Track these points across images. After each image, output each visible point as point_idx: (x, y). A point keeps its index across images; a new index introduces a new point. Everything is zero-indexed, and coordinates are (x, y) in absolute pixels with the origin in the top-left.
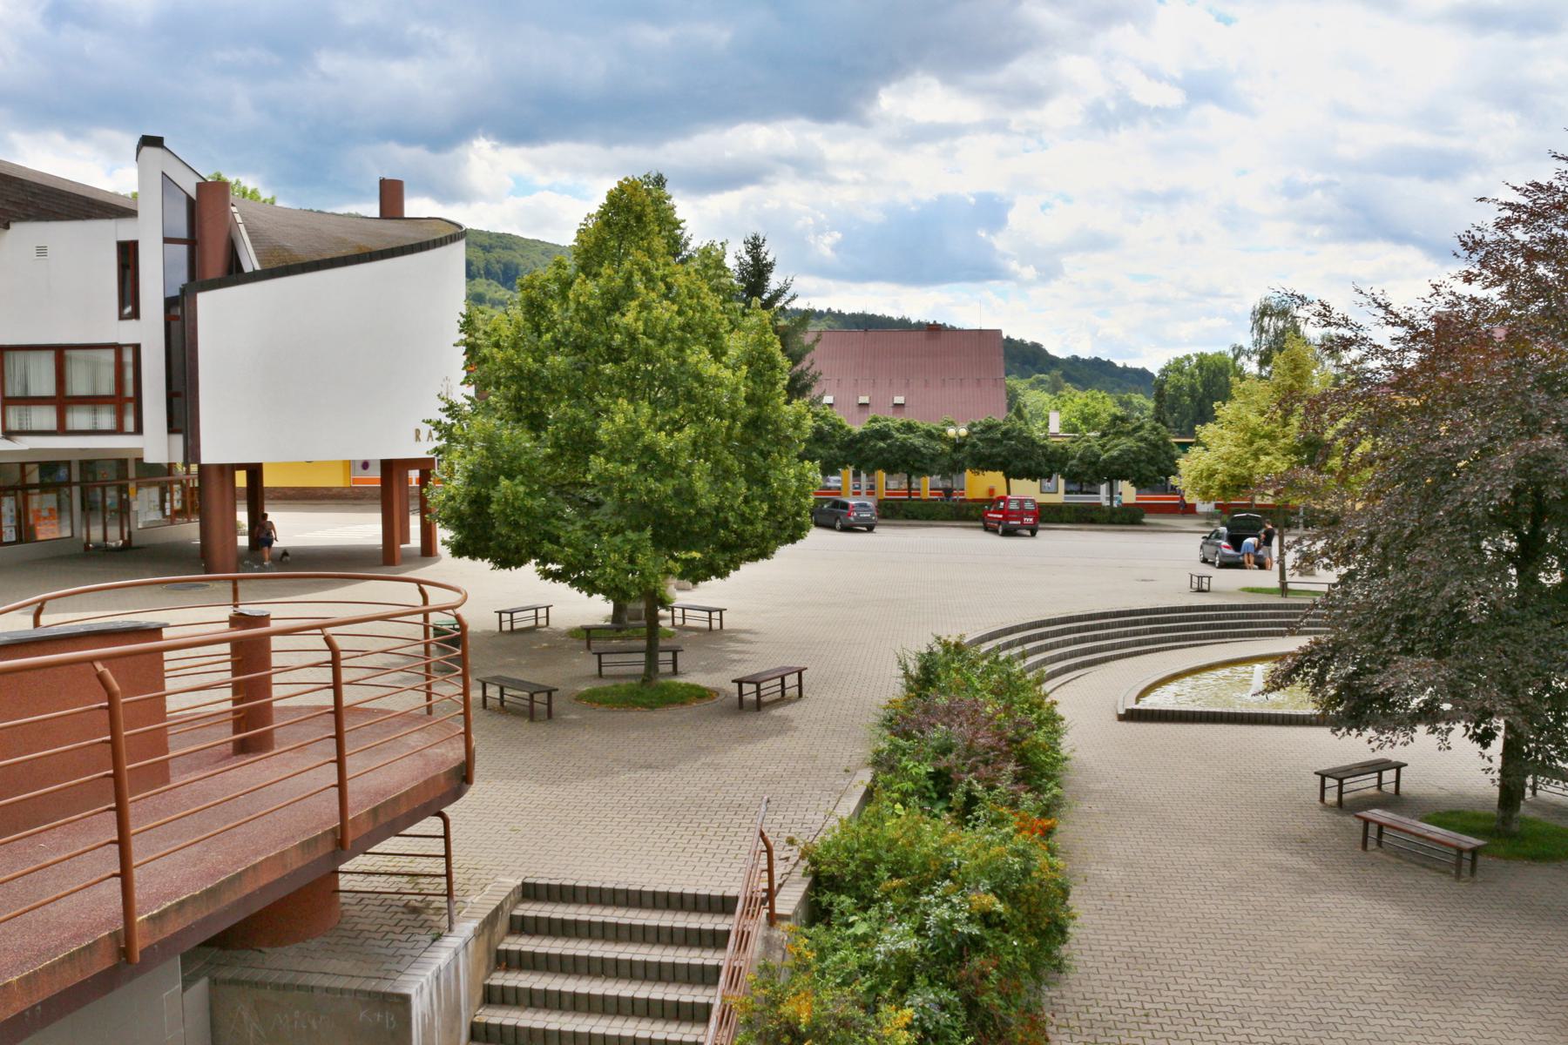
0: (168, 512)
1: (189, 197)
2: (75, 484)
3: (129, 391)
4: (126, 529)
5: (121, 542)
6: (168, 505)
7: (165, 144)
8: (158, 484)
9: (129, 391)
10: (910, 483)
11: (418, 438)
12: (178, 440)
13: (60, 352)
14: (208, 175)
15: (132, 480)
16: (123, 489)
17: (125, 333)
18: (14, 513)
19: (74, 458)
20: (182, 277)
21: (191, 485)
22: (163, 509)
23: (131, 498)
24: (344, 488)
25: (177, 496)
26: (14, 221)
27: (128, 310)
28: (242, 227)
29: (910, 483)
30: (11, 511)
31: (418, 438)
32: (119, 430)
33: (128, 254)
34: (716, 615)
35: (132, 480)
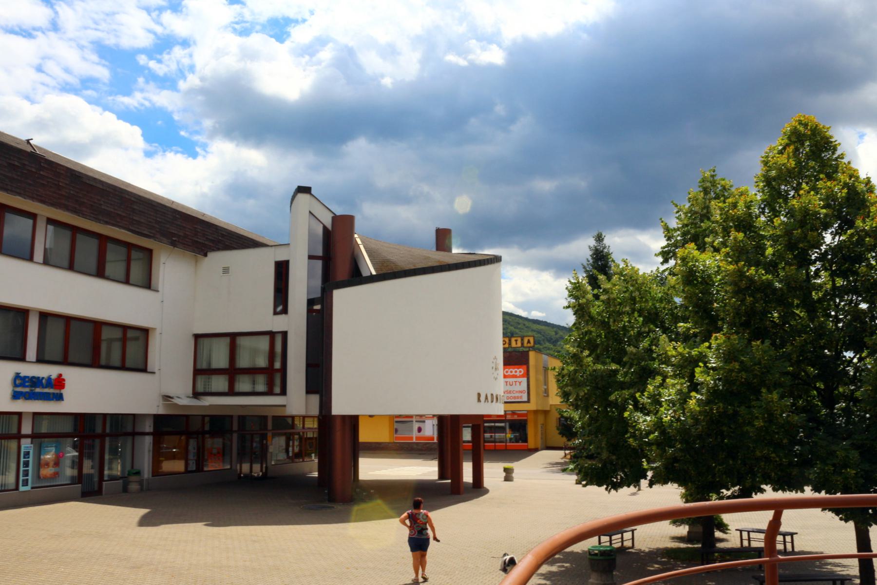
0: (291, 454)
1: (325, 228)
2: (26, 436)
3: (277, 365)
4: (264, 466)
5: (261, 474)
6: (291, 449)
7: (313, 192)
8: (285, 434)
9: (277, 365)
10: (148, 434)
11: (479, 400)
12: (315, 399)
13: (233, 337)
14: (339, 211)
15: (270, 431)
16: (264, 437)
17: (278, 324)
18: (196, 451)
19: (235, 413)
20: (318, 282)
21: (305, 436)
22: (287, 451)
23: (269, 443)
24: (389, 443)
25: (296, 443)
26: (211, 251)
27: (279, 309)
28: (362, 247)
29: (148, 434)
30: (194, 449)
31: (479, 400)
32: (270, 392)
33: (282, 270)
34: (788, 538)
35: (270, 431)
